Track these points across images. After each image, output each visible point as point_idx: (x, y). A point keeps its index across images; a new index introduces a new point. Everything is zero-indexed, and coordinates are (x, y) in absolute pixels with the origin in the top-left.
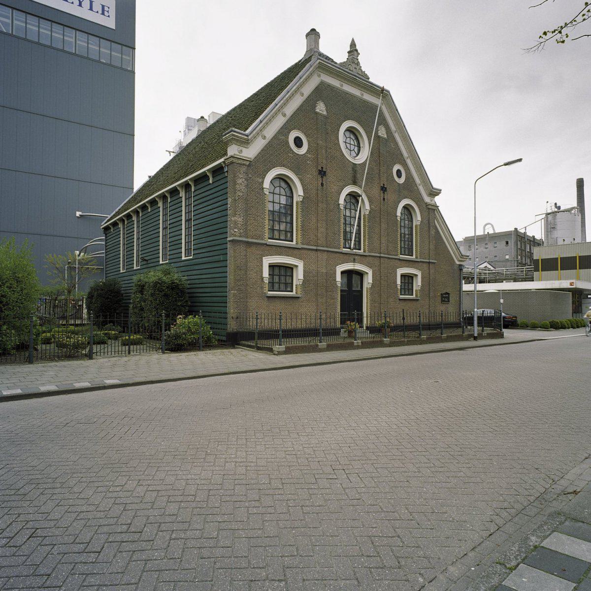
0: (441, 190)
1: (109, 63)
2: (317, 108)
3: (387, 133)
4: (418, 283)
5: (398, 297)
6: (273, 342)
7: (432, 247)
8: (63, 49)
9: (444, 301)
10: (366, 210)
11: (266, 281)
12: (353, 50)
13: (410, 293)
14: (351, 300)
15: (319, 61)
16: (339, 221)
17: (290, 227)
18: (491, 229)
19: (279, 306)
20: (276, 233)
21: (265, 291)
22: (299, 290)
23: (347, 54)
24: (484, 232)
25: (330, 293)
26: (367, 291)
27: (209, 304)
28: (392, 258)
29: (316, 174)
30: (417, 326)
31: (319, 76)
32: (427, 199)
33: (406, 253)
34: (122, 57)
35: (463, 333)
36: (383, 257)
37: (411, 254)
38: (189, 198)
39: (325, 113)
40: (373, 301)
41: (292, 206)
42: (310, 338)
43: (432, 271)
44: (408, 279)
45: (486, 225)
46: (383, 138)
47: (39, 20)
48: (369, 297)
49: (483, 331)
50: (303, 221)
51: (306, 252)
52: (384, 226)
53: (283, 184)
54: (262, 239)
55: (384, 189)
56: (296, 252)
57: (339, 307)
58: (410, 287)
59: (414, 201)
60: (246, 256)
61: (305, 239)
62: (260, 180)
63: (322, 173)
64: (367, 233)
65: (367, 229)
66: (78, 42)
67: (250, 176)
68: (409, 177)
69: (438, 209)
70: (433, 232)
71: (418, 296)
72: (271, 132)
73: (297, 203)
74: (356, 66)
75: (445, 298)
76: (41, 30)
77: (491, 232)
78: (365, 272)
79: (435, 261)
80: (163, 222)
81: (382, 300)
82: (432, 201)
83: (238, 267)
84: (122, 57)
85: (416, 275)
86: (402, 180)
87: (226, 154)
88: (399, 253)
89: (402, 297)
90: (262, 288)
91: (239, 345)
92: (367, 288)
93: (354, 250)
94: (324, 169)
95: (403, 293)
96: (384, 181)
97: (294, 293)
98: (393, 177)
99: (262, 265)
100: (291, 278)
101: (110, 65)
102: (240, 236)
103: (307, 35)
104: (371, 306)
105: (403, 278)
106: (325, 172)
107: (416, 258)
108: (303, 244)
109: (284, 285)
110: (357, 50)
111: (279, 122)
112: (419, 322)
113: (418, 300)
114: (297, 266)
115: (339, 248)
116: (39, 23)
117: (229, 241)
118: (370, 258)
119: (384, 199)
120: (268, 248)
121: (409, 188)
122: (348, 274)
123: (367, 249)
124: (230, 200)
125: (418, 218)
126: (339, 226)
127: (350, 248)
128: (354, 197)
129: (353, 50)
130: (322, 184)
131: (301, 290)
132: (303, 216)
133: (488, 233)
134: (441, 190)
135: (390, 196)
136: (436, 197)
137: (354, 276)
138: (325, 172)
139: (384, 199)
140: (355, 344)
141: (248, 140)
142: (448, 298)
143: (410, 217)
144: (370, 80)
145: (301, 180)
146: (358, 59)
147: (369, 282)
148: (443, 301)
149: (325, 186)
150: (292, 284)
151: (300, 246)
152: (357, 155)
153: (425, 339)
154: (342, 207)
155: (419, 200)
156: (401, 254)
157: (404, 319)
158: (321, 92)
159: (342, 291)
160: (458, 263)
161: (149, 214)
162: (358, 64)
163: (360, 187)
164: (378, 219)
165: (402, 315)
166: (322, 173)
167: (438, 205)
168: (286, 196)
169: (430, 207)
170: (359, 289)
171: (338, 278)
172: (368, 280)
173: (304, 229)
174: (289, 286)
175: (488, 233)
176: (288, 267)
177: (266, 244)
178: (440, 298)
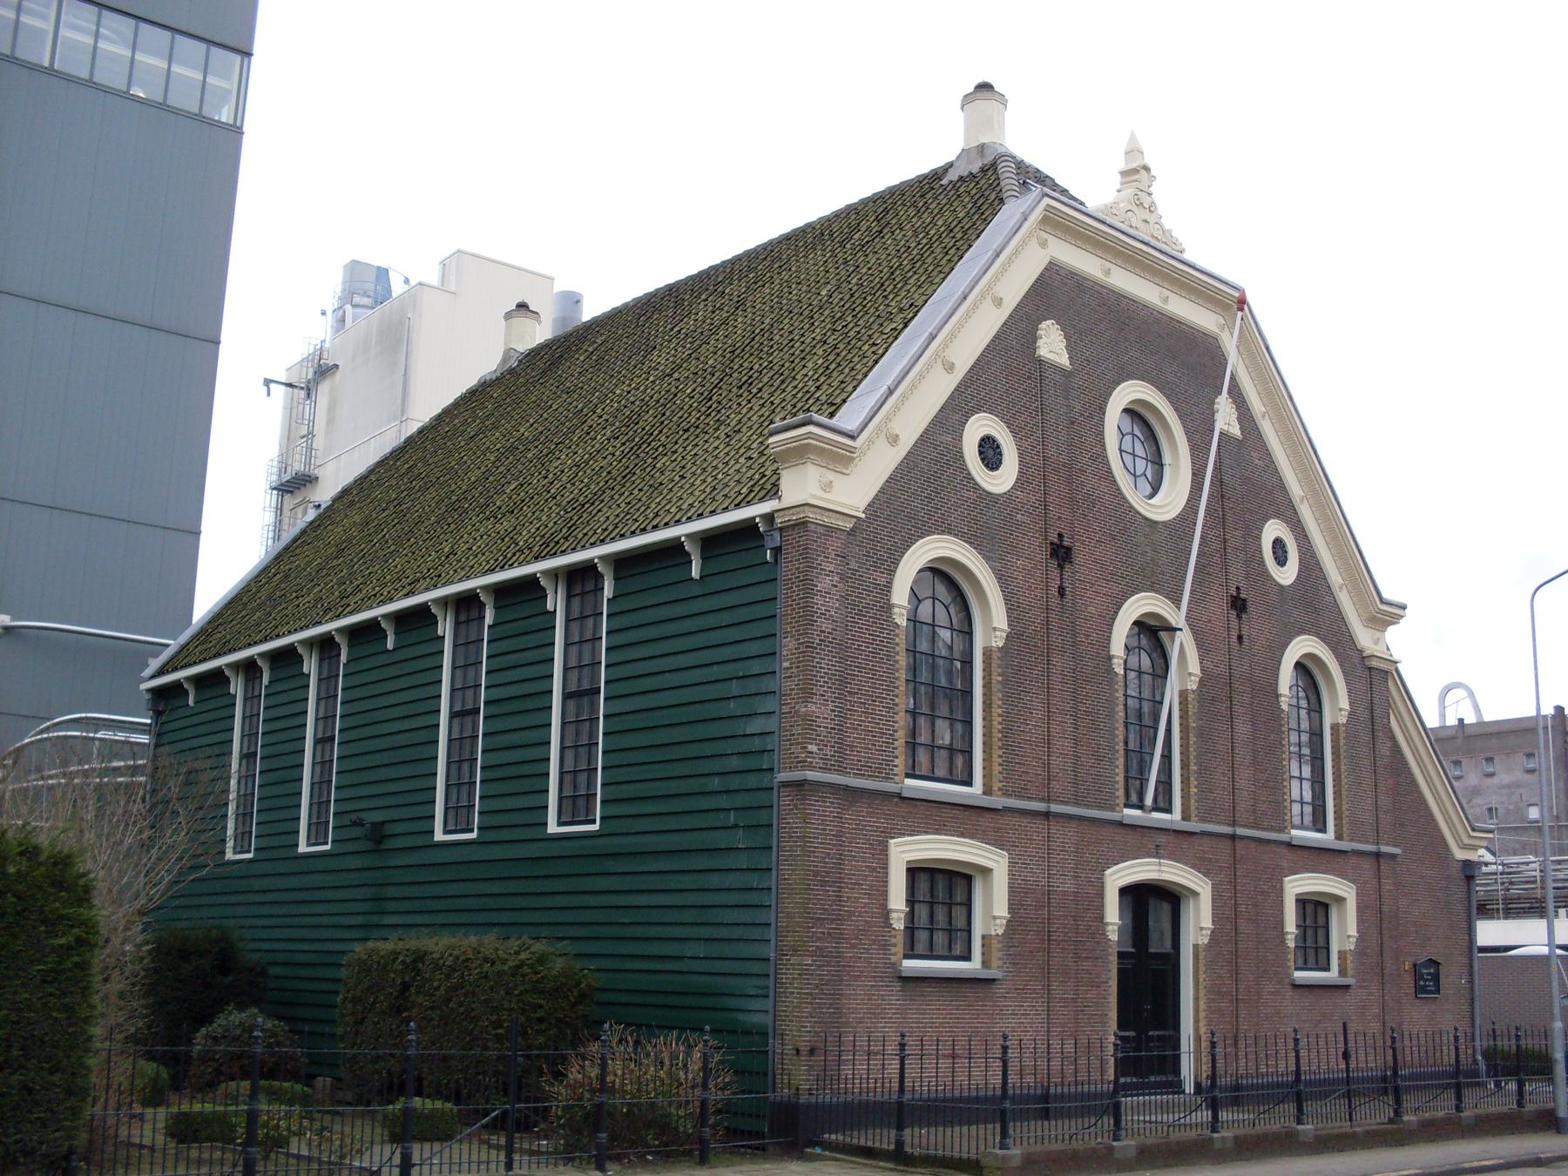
0: (1404, 607)
1: (196, 111)
2: (1040, 343)
3: (1239, 420)
4: (992, 908)
5: (1289, 975)
6: (982, 1132)
7: (1384, 801)
8: (128, 92)
9: (1424, 990)
10: (995, 629)
11: (899, 923)
12: (1136, 173)
13: (958, 949)
14: (1148, 984)
15: (1047, 201)
16: (1111, 715)
17: (963, 737)
18: (1468, 703)
19: (934, 1015)
20: (923, 756)
21: (893, 959)
22: (996, 955)
23: (1118, 178)
24: (1443, 716)
25: (1086, 965)
26: (1196, 957)
27: (690, 1001)
28: (1269, 841)
29: (1042, 554)
30: (993, 1100)
31: (1044, 244)
32: (1364, 638)
33: (940, 772)
34: (95, 47)
35: (1458, 1108)
36: (1243, 838)
37: (1320, 826)
38: (583, 618)
39: (1063, 359)
40: (1214, 992)
41: (968, 663)
42: (1073, 1122)
43: (1387, 885)
44: (944, 888)
45: (1447, 690)
46: (1056, 368)
47: (99, 16)
48: (1202, 977)
49: (1215, 1125)
50: (1006, 716)
51: (1014, 820)
52: (1243, 729)
53: (942, 590)
54: (887, 779)
55: (1238, 604)
56: (985, 821)
57: (1113, 1014)
58: (1321, 943)
59: (1328, 644)
60: (839, 835)
61: (1012, 776)
62: (882, 581)
63: (1061, 553)
64: (1192, 755)
65: (1192, 739)
66: (63, 32)
67: (853, 565)
68: (1310, 566)
69: (1397, 670)
70: (1384, 750)
71: (1350, 972)
72: (913, 419)
73: (987, 653)
74: (1146, 215)
75: (1427, 979)
76: (102, 44)
77: (1470, 719)
78: (1189, 889)
79: (1396, 851)
80: (453, 690)
81: (1242, 987)
82: (1377, 642)
83: (816, 874)
84: (95, 47)
85: (1340, 900)
86: (1286, 575)
87: (774, 491)
88: (1121, 800)
89: (912, 965)
90: (885, 946)
91: (814, 1144)
92: (1196, 947)
93: (1156, 815)
94: (1066, 538)
95: (920, 948)
96: (1237, 576)
97: (973, 967)
98: (1262, 562)
99: (885, 867)
100: (964, 910)
101: (163, 107)
102: (825, 769)
103: (967, 100)
104: (1209, 1009)
105: (923, 884)
106: (1069, 549)
107: (987, 791)
108: (1006, 794)
109: (946, 935)
110: (1146, 169)
111: (936, 391)
112: (1298, 1072)
113: (1347, 987)
114: (986, 871)
115: (1281, 830)
116: (98, 25)
117: (786, 784)
118: (1205, 840)
119: (1240, 638)
120: (903, 809)
121: (1313, 604)
122: (1139, 896)
123: (996, 786)
124: (788, 646)
125: (1338, 704)
126: (1112, 729)
127: (1141, 807)
128: (1151, 631)
129: (1136, 173)
130: (1062, 591)
131: (1000, 954)
132: (1006, 696)
133: (1461, 720)
134: (1404, 607)
135: (1255, 626)
136: (1390, 629)
137: (1152, 903)
138: (1069, 549)
139: (1240, 638)
140: (1217, 1146)
141: (851, 450)
142: (1436, 978)
143: (1313, 698)
144: (1187, 256)
145: (1001, 578)
146: (1150, 194)
147: (996, 913)
148: (1419, 990)
149: (1069, 597)
150: (969, 932)
151: (998, 801)
152: (1155, 490)
153: (1230, 1144)
154: (901, 618)
155: (1341, 641)
156: (1127, 806)
157: (1346, 1056)
158: (1054, 293)
159: (1121, 955)
160: (1460, 855)
161: (381, 660)
162: (1151, 209)
163: (1177, 602)
164: (1223, 707)
165: (1341, 1045)
166: (1061, 553)
167: (1396, 657)
168: (952, 629)
169: (1374, 663)
170: (1167, 946)
171: (1113, 913)
172: (1199, 922)
173: (1007, 741)
174: (957, 941)
175: (1461, 720)
176: (958, 874)
177: (899, 796)
178: (1409, 980)
